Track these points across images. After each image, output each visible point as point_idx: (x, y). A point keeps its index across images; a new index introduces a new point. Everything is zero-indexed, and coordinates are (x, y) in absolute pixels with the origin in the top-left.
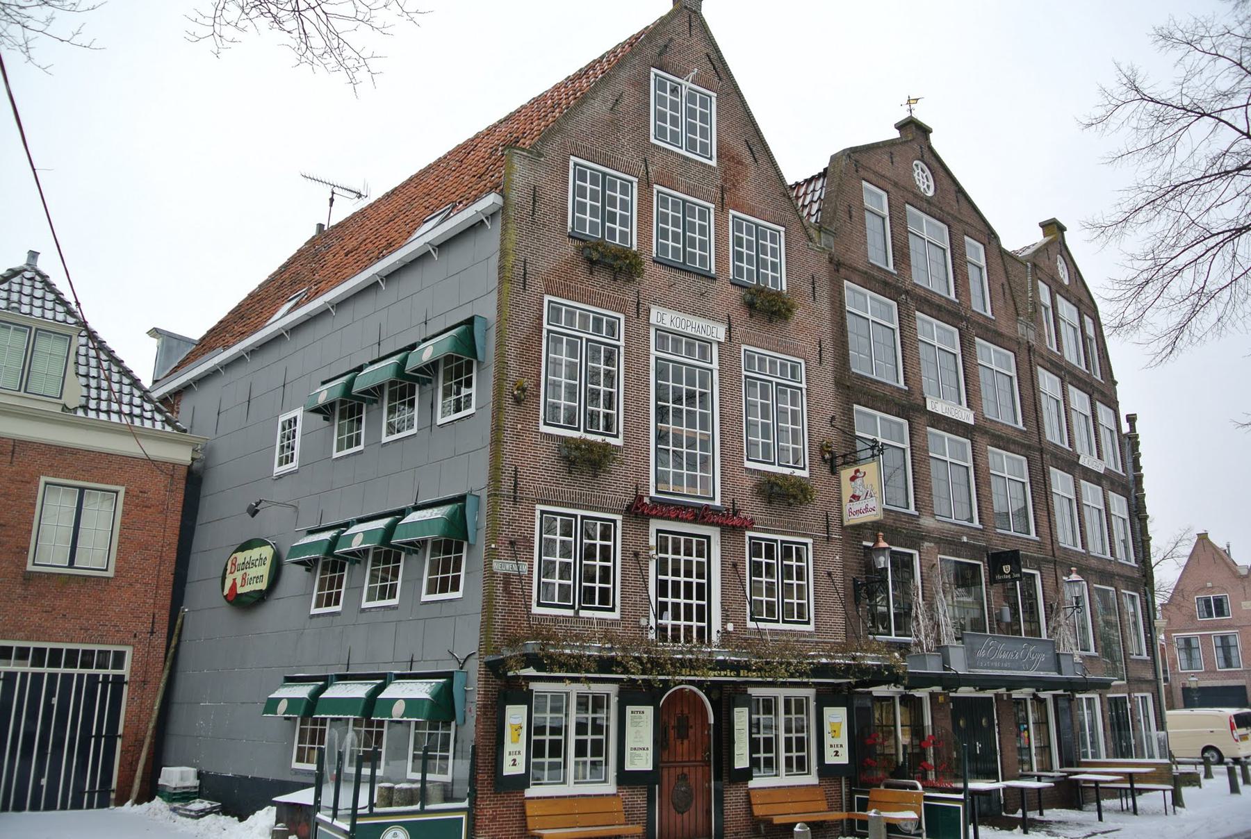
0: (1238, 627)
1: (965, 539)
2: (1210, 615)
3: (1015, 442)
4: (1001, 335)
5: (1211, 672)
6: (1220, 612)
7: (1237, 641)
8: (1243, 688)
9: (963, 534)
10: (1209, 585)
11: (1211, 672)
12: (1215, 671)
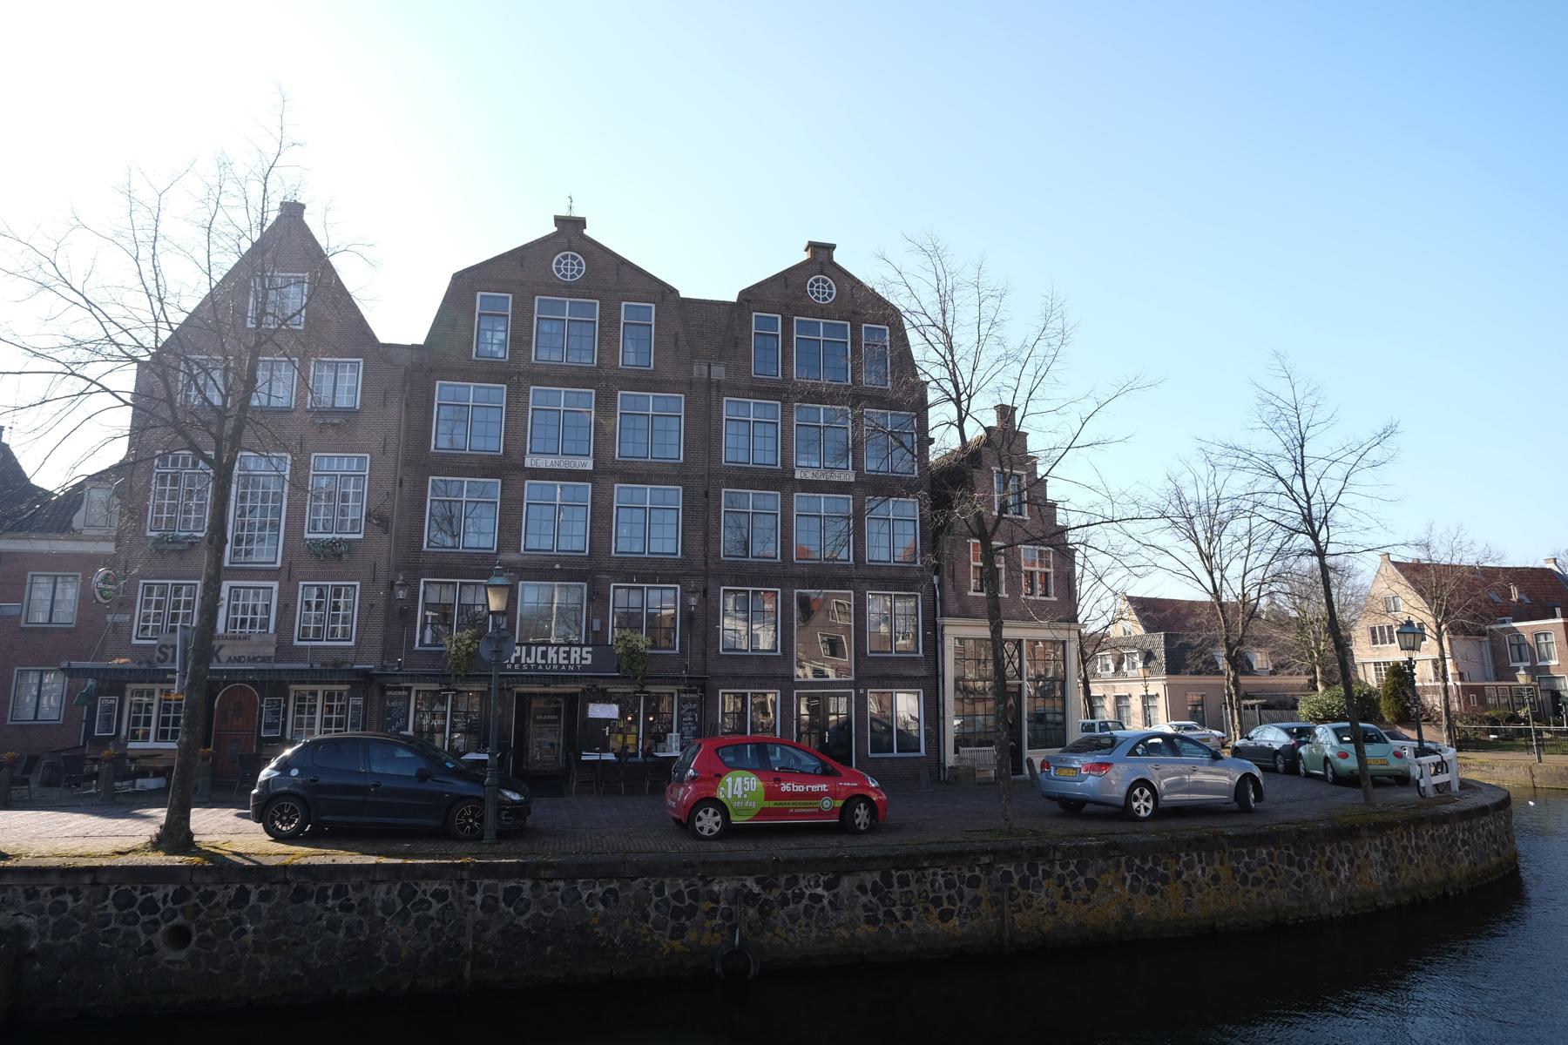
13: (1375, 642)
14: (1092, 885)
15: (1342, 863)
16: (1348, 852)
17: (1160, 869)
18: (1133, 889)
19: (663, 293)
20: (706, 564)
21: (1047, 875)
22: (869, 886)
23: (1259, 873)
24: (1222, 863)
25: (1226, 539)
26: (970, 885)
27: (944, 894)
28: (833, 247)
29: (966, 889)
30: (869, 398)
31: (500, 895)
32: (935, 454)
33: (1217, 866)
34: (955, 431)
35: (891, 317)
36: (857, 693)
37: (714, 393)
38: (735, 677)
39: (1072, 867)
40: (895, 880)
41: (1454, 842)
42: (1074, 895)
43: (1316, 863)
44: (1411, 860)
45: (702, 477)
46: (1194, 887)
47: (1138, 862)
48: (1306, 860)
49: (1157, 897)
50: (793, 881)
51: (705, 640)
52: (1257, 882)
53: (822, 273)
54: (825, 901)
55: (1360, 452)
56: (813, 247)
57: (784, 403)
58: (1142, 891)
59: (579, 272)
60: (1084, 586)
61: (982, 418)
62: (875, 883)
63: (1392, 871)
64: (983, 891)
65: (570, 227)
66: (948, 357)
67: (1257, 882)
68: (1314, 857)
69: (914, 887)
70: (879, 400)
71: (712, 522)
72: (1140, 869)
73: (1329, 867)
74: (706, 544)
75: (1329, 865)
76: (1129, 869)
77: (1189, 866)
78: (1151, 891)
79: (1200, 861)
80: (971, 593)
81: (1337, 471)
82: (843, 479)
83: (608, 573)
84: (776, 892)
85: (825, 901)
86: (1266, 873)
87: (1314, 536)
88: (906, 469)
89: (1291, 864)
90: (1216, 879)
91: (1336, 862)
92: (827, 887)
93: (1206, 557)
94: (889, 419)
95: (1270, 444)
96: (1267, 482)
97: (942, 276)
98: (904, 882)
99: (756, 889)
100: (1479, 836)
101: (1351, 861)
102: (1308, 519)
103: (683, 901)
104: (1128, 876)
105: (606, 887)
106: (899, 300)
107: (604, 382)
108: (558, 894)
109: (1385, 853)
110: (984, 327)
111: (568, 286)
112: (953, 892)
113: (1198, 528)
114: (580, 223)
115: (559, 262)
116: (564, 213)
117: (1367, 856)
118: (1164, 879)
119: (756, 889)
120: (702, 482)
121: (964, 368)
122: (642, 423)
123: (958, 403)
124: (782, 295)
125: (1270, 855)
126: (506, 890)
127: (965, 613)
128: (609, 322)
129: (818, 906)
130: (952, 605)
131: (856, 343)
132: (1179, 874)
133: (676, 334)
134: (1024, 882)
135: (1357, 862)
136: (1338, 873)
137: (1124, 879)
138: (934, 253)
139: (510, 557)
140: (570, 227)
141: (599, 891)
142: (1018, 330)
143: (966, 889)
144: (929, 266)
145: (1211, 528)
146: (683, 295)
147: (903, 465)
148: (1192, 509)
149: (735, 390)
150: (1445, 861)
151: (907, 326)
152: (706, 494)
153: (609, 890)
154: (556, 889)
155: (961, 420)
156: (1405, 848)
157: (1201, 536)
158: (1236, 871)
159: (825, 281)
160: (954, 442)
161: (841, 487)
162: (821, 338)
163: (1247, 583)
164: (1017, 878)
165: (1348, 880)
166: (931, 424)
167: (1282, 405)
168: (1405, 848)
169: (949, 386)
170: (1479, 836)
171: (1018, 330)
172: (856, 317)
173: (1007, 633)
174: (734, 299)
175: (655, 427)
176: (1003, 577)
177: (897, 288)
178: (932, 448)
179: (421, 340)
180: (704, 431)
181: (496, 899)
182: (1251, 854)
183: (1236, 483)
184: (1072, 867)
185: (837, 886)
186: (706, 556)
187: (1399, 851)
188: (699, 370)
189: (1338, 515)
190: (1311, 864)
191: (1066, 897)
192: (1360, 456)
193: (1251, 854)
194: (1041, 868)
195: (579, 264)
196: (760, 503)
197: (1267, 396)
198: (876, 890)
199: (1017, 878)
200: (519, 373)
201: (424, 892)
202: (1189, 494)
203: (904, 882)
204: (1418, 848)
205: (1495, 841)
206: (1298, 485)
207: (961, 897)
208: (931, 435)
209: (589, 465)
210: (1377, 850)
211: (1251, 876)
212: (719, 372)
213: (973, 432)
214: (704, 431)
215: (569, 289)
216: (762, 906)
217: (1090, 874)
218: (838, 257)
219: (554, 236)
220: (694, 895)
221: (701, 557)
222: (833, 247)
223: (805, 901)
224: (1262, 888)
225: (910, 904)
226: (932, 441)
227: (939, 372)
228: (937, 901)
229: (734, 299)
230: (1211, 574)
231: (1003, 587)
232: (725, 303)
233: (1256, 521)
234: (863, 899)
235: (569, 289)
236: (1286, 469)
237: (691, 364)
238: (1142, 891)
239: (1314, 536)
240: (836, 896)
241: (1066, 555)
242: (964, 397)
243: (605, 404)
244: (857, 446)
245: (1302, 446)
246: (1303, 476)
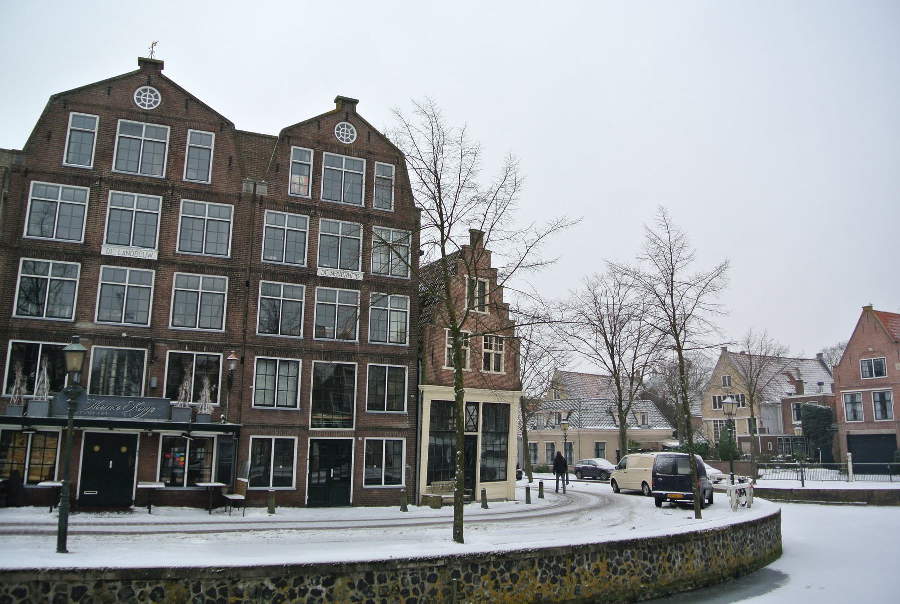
0: (892, 385)
1: (124, 335)
2: (872, 376)
3: (217, 268)
4: (216, 194)
5: (869, 422)
6: (880, 373)
7: (891, 397)
8: (893, 437)
9: (125, 332)
10: (871, 350)
11: (869, 422)
12: (873, 422)
13: (715, 407)
14: (514, 578)
15: (677, 558)
16: (681, 549)
17: (561, 566)
18: (543, 581)
19: (222, 125)
20: (244, 338)
21: (484, 572)
22: (357, 584)
23: (625, 567)
24: (602, 561)
25: (624, 334)
26: (429, 581)
27: (411, 587)
28: (356, 102)
29: (427, 584)
30: (377, 218)
31: (69, 593)
32: (424, 261)
33: (598, 562)
34: (438, 249)
35: (397, 157)
36: (357, 440)
37: (258, 206)
38: (264, 426)
39: (502, 567)
40: (376, 578)
41: (745, 541)
42: (502, 585)
43: (661, 558)
44: (719, 554)
45: (245, 270)
46: (582, 578)
47: (546, 562)
48: (655, 556)
49: (558, 585)
50: (301, 580)
51: (241, 397)
52: (624, 572)
53: (347, 121)
54: (324, 595)
55: (707, 281)
56: (340, 101)
57: (312, 217)
58: (548, 582)
59: (156, 103)
60: (525, 366)
61: (460, 237)
62: (361, 581)
63: (707, 562)
64: (438, 585)
65: (151, 69)
66: (438, 195)
67: (624, 572)
68: (660, 554)
69: (390, 584)
70: (387, 221)
71: (251, 306)
72: (548, 566)
73: (669, 561)
74: (245, 323)
75: (669, 559)
76: (541, 566)
77: (580, 563)
78: (554, 581)
79: (588, 560)
80: (445, 368)
81: (692, 293)
82: (354, 278)
83: (165, 342)
84: (287, 589)
85: (324, 595)
86: (629, 566)
87: (677, 337)
88: (402, 274)
89: (645, 559)
90: (597, 571)
91: (673, 557)
92: (326, 584)
93: (611, 347)
94: (394, 235)
95: (651, 270)
96: (651, 297)
97: (436, 132)
98: (382, 580)
99: (272, 587)
100: (761, 536)
101: (683, 556)
102: (674, 326)
103: (215, 597)
104: (540, 571)
105: (155, 587)
106: (406, 148)
107: (170, 190)
108: (117, 592)
109: (704, 550)
110: (464, 174)
111: (146, 113)
112: (417, 586)
113: (607, 325)
114: (160, 65)
115: (140, 94)
116: (146, 55)
117: (693, 552)
118: (564, 573)
119: (272, 587)
120: (244, 272)
121: (448, 203)
122: (198, 225)
123: (442, 228)
124: (312, 134)
125: (633, 554)
126: (74, 589)
127: (439, 382)
128: (178, 143)
129: (318, 599)
130: (432, 376)
131: (370, 175)
132: (573, 569)
133: (231, 158)
134: (468, 579)
135: (686, 556)
136: (674, 563)
137: (537, 574)
138: (434, 118)
139: (84, 326)
140: (151, 69)
141: (149, 589)
142: (486, 180)
143: (427, 584)
144: (428, 125)
145: (615, 326)
146: (238, 127)
147: (399, 271)
148: (604, 311)
149: (275, 204)
150: (740, 554)
151: (409, 166)
152: (248, 284)
153: (157, 589)
154: (115, 588)
155: (443, 242)
156: (716, 546)
157: (608, 330)
158: (609, 565)
159: (349, 127)
160: (438, 256)
161: (353, 284)
162: (344, 170)
163: (636, 366)
164: (463, 575)
165: (680, 568)
166: (423, 241)
167: (662, 245)
168: (716, 546)
169: (436, 215)
170: (761, 536)
171: (486, 180)
172: (370, 157)
173: (467, 399)
174: (277, 134)
175: (210, 227)
176: (468, 357)
177: (403, 137)
178: (422, 258)
179: (20, 147)
180: (248, 234)
181: (66, 596)
182: (621, 555)
183: (632, 297)
184: (502, 567)
185: (333, 583)
186: (245, 332)
187: (712, 548)
188: (247, 187)
189: (692, 325)
190: (658, 558)
191: (497, 587)
192: (707, 285)
193: (621, 555)
194: (480, 568)
195: (156, 97)
196: (290, 293)
197: (653, 237)
198: (362, 586)
199: (463, 575)
200: (101, 180)
201: (7, 591)
202: (603, 300)
203: (382, 580)
204: (724, 546)
205: (770, 539)
206: (668, 301)
207: (423, 589)
208: (422, 249)
209: (155, 257)
210: (699, 548)
211: (619, 568)
212: (263, 190)
213: (450, 249)
214: (248, 234)
215: (147, 116)
216: (276, 600)
217: (514, 571)
218: (360, 110)
219: (137, 73)
220: (224, 592)
221: (241, 332)
222: (356, 102)
223: (309, 595)
224: (626, 577)
225: (386, 596)
226: (422, 253)
227: (430, 204)
228: (406, 593)
229: (277, 134)
230: (613, 359)
231: (468, 363)
232: (270, 137)
233: (643, 323)
234: (352, 593)
235: (147, 116)
236: (661, 289)
237: (242, 182)
238: (548, 582)
239: (677, 337)
240: (331, 591)
241: (514, 343)
242: (446, 225)
243: (170, 207)
244: (367, 251)
245: (672, 274)
246: (672, 295)
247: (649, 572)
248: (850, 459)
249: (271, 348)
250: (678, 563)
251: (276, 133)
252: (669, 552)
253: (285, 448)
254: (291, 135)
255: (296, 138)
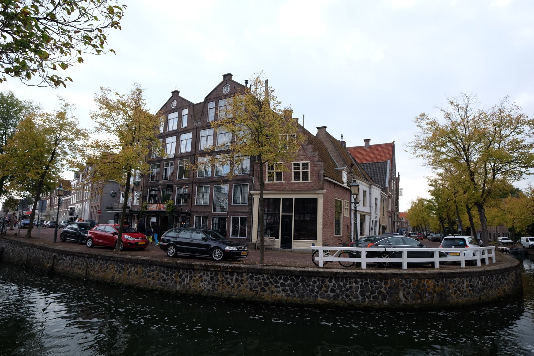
23: (151, 274)
38: (198, 212)
52: (149, 276)
89: (163, 273)
101: (191, 277)
109: (212, 278)
124: (215, 95)
134: (94, 264)
137: (115, 267)
211: (148, 274)
224: (150, 279)
247: (165, 280)
248: (26, 222)
249: (228, 152)
250: (187, 280)
251: (203, 100)
252: (181, 272)
253: (235, 233)
254: (208, 99)
255: (208, 101)
